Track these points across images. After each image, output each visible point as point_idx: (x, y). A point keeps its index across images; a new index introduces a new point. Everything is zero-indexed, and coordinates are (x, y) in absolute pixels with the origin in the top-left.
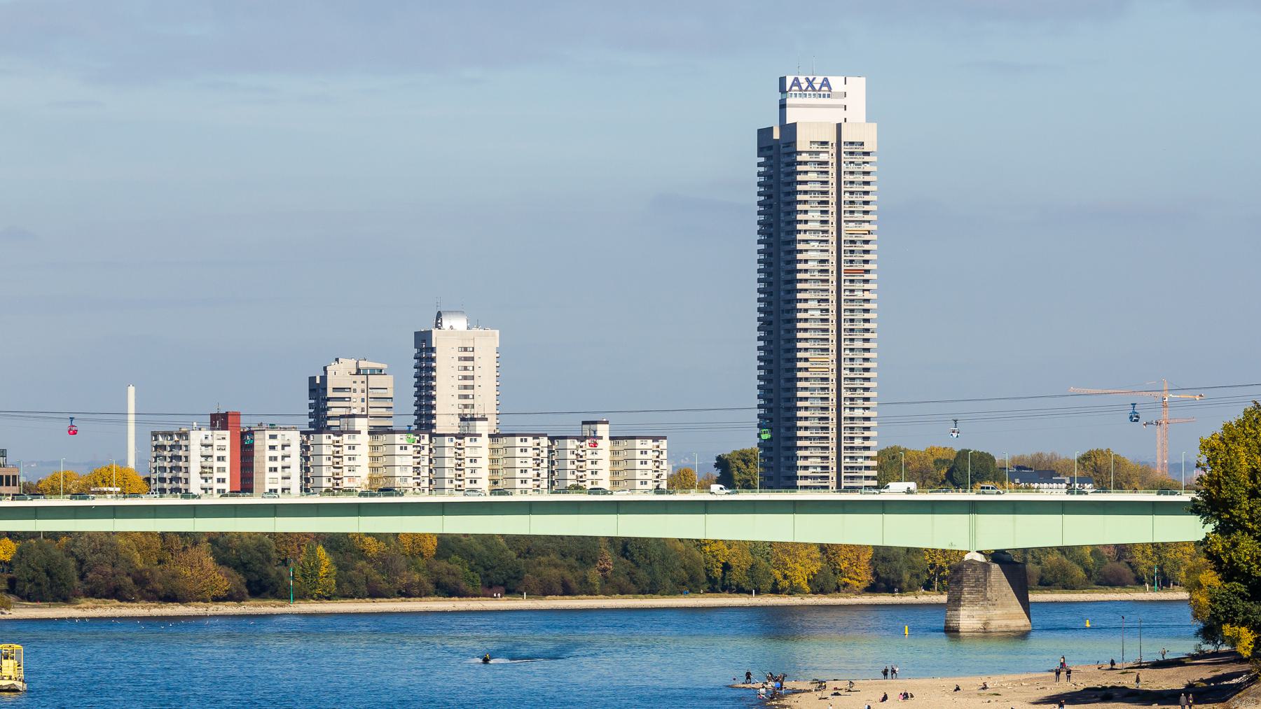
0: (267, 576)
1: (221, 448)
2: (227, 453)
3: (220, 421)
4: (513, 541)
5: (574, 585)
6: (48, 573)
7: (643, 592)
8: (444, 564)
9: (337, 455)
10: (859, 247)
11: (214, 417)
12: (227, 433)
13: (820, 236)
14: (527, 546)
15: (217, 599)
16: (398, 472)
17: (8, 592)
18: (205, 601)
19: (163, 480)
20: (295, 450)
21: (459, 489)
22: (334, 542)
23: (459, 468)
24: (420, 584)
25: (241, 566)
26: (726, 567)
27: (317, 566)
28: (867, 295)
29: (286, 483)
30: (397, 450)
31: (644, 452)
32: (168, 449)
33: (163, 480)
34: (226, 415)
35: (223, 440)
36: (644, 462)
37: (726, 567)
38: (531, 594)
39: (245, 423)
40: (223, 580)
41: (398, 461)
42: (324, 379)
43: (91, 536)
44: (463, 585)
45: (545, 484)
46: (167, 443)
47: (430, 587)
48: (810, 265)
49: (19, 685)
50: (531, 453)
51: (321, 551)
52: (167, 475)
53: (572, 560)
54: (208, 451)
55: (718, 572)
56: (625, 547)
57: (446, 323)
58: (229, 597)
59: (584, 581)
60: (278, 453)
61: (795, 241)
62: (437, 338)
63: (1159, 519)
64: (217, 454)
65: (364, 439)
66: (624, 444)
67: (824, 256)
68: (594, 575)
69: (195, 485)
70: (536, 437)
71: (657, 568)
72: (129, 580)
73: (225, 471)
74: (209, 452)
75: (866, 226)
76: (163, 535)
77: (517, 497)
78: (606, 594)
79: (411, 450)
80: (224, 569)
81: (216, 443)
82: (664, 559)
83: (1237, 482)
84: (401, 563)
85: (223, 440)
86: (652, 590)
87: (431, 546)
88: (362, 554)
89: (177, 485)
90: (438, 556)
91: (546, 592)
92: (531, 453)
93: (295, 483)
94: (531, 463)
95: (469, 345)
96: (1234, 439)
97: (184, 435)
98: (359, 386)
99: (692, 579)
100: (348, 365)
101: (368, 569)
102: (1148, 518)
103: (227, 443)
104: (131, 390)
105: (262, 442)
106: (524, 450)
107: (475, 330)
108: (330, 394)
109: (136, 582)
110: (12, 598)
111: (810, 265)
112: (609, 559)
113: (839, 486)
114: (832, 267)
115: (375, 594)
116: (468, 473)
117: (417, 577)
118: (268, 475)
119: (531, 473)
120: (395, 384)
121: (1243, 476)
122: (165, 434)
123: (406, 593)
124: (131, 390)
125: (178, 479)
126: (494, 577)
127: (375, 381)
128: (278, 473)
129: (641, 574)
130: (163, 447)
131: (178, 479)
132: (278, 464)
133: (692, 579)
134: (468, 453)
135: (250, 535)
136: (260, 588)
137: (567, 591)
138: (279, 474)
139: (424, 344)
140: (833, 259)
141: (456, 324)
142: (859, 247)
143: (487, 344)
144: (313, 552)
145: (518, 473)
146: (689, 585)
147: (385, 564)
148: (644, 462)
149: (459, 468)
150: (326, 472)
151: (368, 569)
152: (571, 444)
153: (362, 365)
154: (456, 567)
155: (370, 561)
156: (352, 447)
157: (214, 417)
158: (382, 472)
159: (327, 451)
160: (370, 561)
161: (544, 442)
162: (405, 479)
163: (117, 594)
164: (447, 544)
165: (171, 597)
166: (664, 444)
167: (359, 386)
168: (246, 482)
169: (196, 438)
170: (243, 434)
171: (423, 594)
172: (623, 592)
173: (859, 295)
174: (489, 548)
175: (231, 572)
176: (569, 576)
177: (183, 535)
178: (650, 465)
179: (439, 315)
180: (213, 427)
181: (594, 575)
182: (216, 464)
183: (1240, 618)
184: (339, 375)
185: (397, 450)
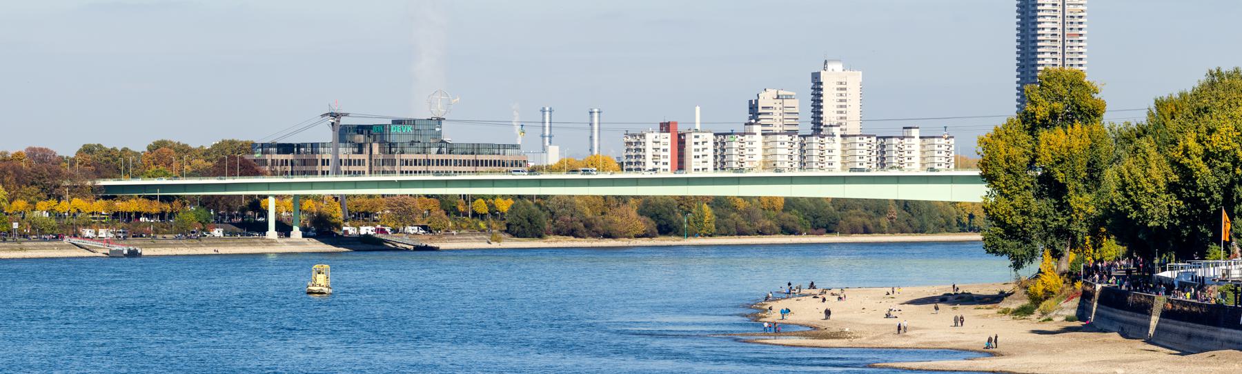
0: (671, 222)
1: (665, 144)
2: (669, 147)
3: (665, 127)
4: (835, 201)
5: (871, 227)
6: (529, 220)
7: (915, 232)
8: (787, 215)
9: (901, 150)
10: (1076, 20)
11: (662, 125)
12: (669, 135)
13: (1052, 14)
14: (843, 205)
15: (637, 236)
16: (779, 158)
17: (506, 231)
18: (629, 237)
19: (631, 163)
20: (710, 145)
21: (821, 168)
22: (717, 202)
23: (821, 156)
24: (771, 227)
25: (655, 216)
26: (971, 216)
27: (703, 216)
28: (1081, 50)
29: (705, 165)
30: (778, 145)
31: (940, 146)
32: (635, 145)
33: (631, 163)
34: (668, 124)
35: (667, 139)
36: (940, 152)
37: (971, 216)
38: (842, 233)
39: (681, 129)
40: (641, 224)
41: (779, 151)
42: (757, 101)
43: (558, 198)
44: (799, 228)
45: (796, 165)
46: (633, 140)
47: (778, 229)
48: (1046, 31)
49: (326, 290)
50: (865, 146)
51: (706, 207)
52: (633, 160)
53: (871, 213)
54: (657, 146)
55: (966, 220)
56: (905, 205)
57: (830, 66)
58: (645, 235)
59: (879, 225)
60: (700, 146)
61: (1036, 17)
62: (824, 77)
63: (847, 186)
64: (662, 147)
65: (917, 142)
66: (928, 141)
67: (1054, 26)
68: (884, 221)
69: (650, 164)
70: (869, 136)
71: (925, 217)
72: (581, 225)
73: (668, 156)
74: (658, 146)
75: (1081, 8)
76: (605, 197)
77: (787, 174)
78: (892, 233)
79: (787, 145)
80: (644, 218)
81: (662, 141)
82: (929, 211)
83: (997, 164)
84: (759, 213)
85: (667, 139)
86: (922, 231)
87: (780, 204)
88: (735, 209)
89: (639, 165)
90: (784, 210)
91: (854, 231)
92: (865, 146)
93: (710, 165)
94: (866, 153)
95: (843, 80)
96: (999, 137)
97: (642, 136)
98: (778, 106)
99: (948, 224)
100: (772, 93)
101: (738, 218)
102: (948, 186)
103: (669, 140)
104: (698, 109)
105: (690, 140)
106: (861, 145)
107: (847, 72)
108: (760, 110)
109: (586, 226)
110: (507, 235)
111: (1046, 31)
112: (895, 212)
113: (370, 172)
114: (1059, 32)
115: (741, 233)
116: (827, 159)
117: (768, 223)
118: (694, 160)
119: (866, 159)
120: (801, 105)
121: (1002, 161)
122: (632, 135)
123: (761, 233)
124: (698, 109)
125: (639, 163)
126: (820, 222)
127: (787, 103)
128: (701, 161)
129: (915, 221)
130: (631, 143)
131: (639, 163)
132: (700, 153)
133: (948, 224)
134: (827, 147)
135: (661, 197)
136: (666, 229)
137: (866, 231)
138: (701, 159)
139: (816, 78)
140: (1060, 27)
141: (836, 67)
142: (1076, 20)
143: (854, 81)
144: (700, 208)
145: (857, 159)
146: (947, 227)
147: (748, 214)
148: (940, 152)
149: (821, 156)
150: (735, 158)
151: (738, 218)
152: (895, 141)
153: (781, 93)
154: (794, 217)
155: (740, 213)
156: (751, 143)
157: (662, 125)
158: (770, 158)
159: (815, 146)
160: (740, 213)
161: (874, 139)
162: (783, 162)
163: (573, 233)
164: (790, 203)
165: (608, 235)
166: (952, 141)
167: (778, 106)
168: (681, 165)
169: (650, 138)
170: (679, 136)
171: (773, 233)
172: (902, 232)
173: (1076, 49)
174: (817, 205)
175: (648, 219)
176: (868, 222)
177: (617, 197)
178: (944, 154)
179: (826, 62)
180: (661, 131)
181: (884, 221)
182: (662, 154)
183: (1001, 250)
184: (766, 99)
185: (778, 145)
